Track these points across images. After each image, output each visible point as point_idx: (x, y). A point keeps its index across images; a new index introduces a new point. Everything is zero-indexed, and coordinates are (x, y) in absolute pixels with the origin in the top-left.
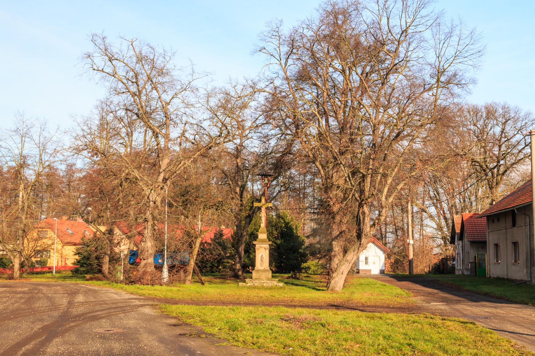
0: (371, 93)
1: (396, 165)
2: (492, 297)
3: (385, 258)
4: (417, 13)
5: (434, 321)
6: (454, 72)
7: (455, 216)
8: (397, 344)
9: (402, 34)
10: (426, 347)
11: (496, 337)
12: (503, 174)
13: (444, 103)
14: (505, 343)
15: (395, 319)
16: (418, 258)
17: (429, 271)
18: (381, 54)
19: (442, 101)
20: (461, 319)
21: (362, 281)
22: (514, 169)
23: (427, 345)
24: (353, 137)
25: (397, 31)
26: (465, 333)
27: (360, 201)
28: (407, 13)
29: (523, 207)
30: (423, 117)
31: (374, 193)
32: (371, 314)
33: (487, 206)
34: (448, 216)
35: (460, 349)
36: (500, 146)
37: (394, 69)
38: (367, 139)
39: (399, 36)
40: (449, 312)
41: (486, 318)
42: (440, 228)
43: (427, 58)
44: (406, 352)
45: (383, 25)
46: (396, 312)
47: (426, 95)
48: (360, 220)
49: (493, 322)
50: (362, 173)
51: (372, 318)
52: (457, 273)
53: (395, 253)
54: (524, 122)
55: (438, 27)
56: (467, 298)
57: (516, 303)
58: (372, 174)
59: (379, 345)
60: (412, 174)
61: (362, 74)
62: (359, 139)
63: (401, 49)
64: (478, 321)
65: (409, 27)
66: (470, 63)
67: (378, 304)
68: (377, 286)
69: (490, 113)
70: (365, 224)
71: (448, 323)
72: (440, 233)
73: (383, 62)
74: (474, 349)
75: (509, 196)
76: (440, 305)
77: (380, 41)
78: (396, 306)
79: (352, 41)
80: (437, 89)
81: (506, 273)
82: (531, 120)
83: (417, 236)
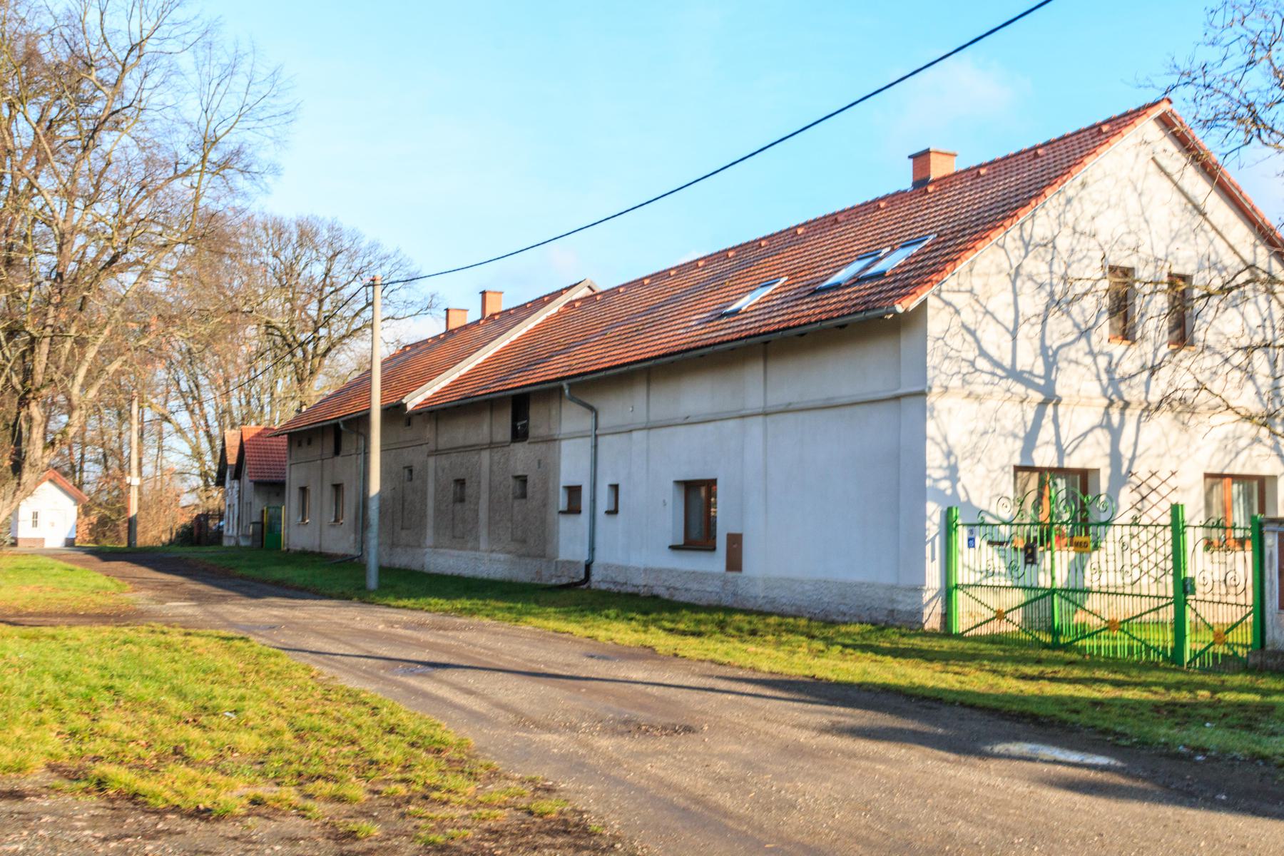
0: (57, 165)
1: (107, 323)
2: (288, 588)
3: (79, 514)
4: (165, 14)
5: (169, 638)
6: (237, 146)
7: (228, 432)
8: (83, 689)
9: (131, 50)
10: (144, 691)
11: (285, 662)
12: (324, 355)
13: (214, 206)
14: (302, 673)
15: (86, 639)
16: (148, 514)
17: (171, 540)
18: (84, 86)
19: (209, 201)
20: (223, 633)
21: (21, 562)
22: (345, 347)
23: (146, 687)
24: (13, 254)
25: (120, 44)
26: (227, 657)
27: (22, 393)
28: (143, 9)
29: (354, 418)
30: (170, 228)
31: (56, 377)
32: (32, 631)
33: (293, 415)
34: (215, 431)
35: (212, 690)
36: (321, 301)
37: (111, 120)
38: (44, 263)
39: (125, 54)
40: (202, 620)
41: (272, 628)
42: (197, 455)
43: (182, 110)
44: (101, 702)
45: (91, 24)
46: (90, 624)
47: (177, 184)
48: (20, 432)
49: (284, 635)
50: (30, 334)
51: (35, 638)
52: (226, 543)
53: (100, 505)
54: (366, 260)
55: (207, 51)
56: (241, 592)
57: (331, 597)
58: (52, 337)
59: (42, 693)
60: (141, 343)
61: (38, 122)
62: (26, 260)
63: (127, 81)
64: (256, 634)
65: (148, 38)
66: (269, 132)
67: (53, 608)
68: (54, 572)
69: (306, 236)
70: (31, 442)
71: (195, 641)
72: (197, 465)
73: (88, 102)
74: (239, 687)
75: (331, 396)
76: (184, 606)
77: (81, 57)
78: (92, 612)
79: (20, 46)
80: (201, 176)
81: (317, 543)
82: (379, 257)
83: (148, 469)
